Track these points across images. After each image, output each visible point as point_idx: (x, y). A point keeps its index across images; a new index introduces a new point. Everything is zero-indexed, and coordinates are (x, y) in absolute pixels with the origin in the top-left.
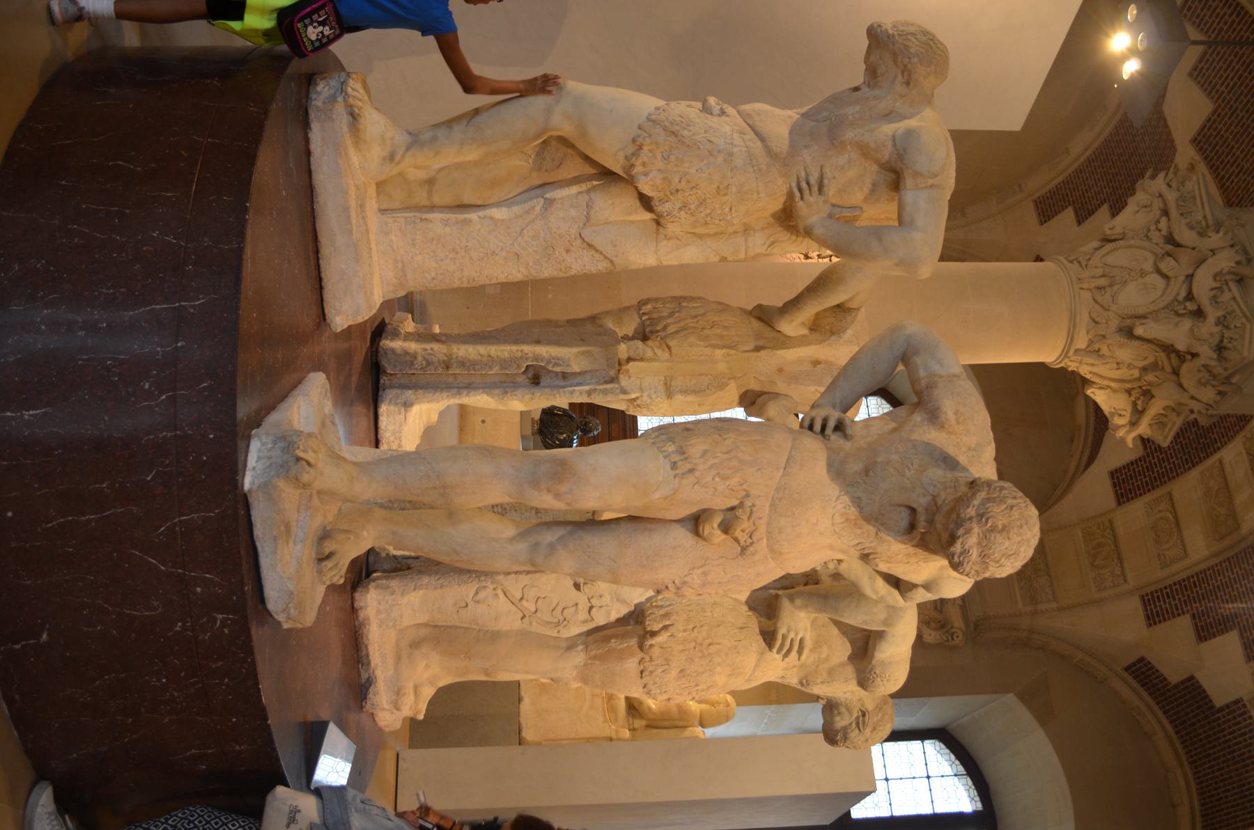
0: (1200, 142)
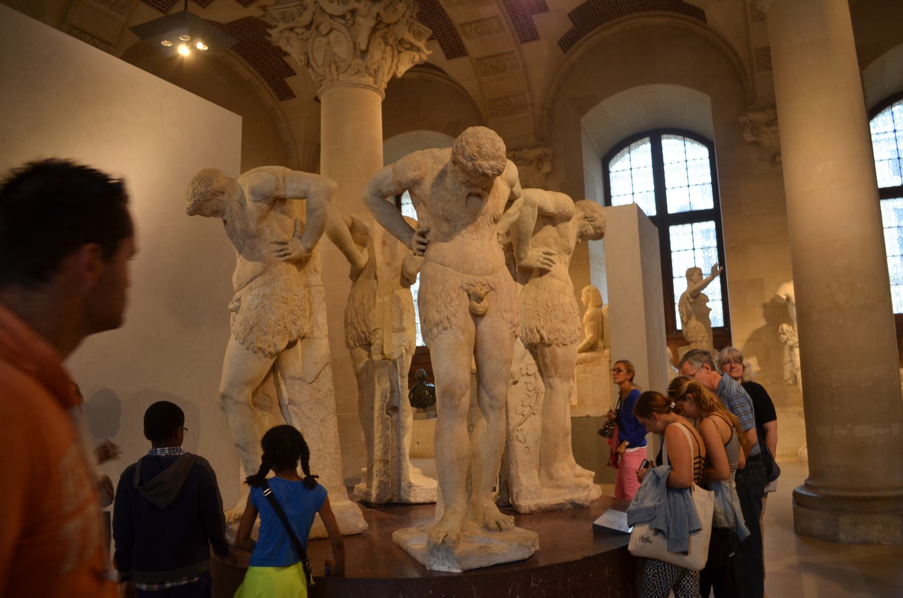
0: (246, 2)
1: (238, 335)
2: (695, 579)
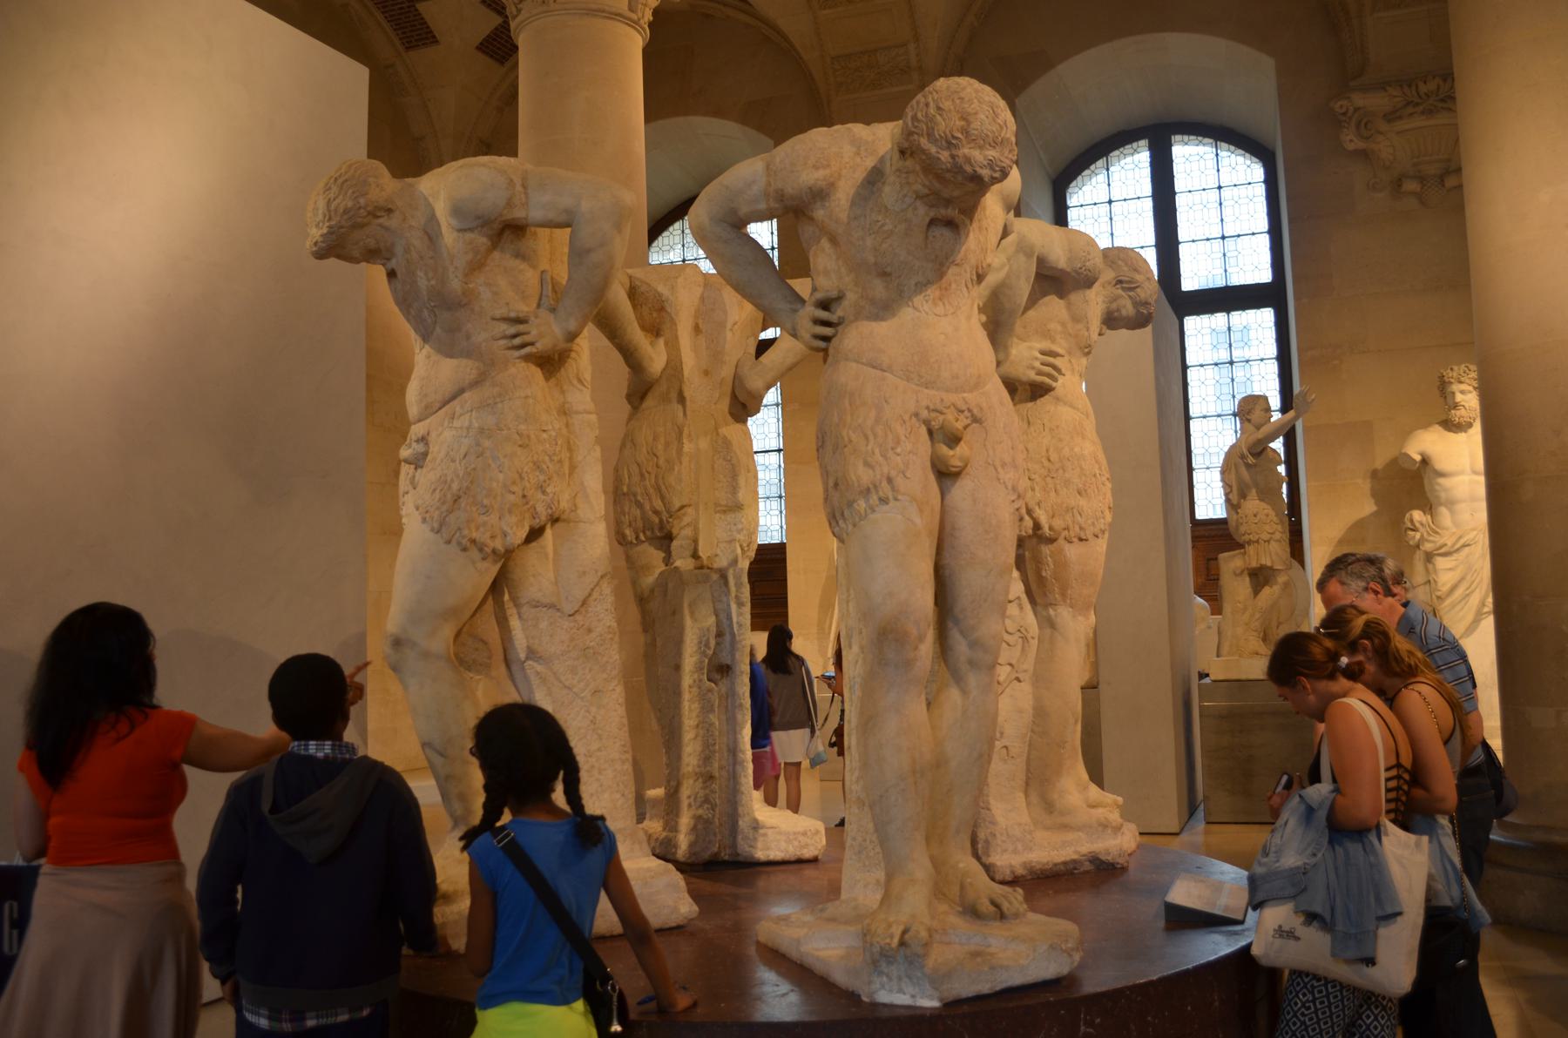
1: (427, 512)
2: (1389, 1012)
